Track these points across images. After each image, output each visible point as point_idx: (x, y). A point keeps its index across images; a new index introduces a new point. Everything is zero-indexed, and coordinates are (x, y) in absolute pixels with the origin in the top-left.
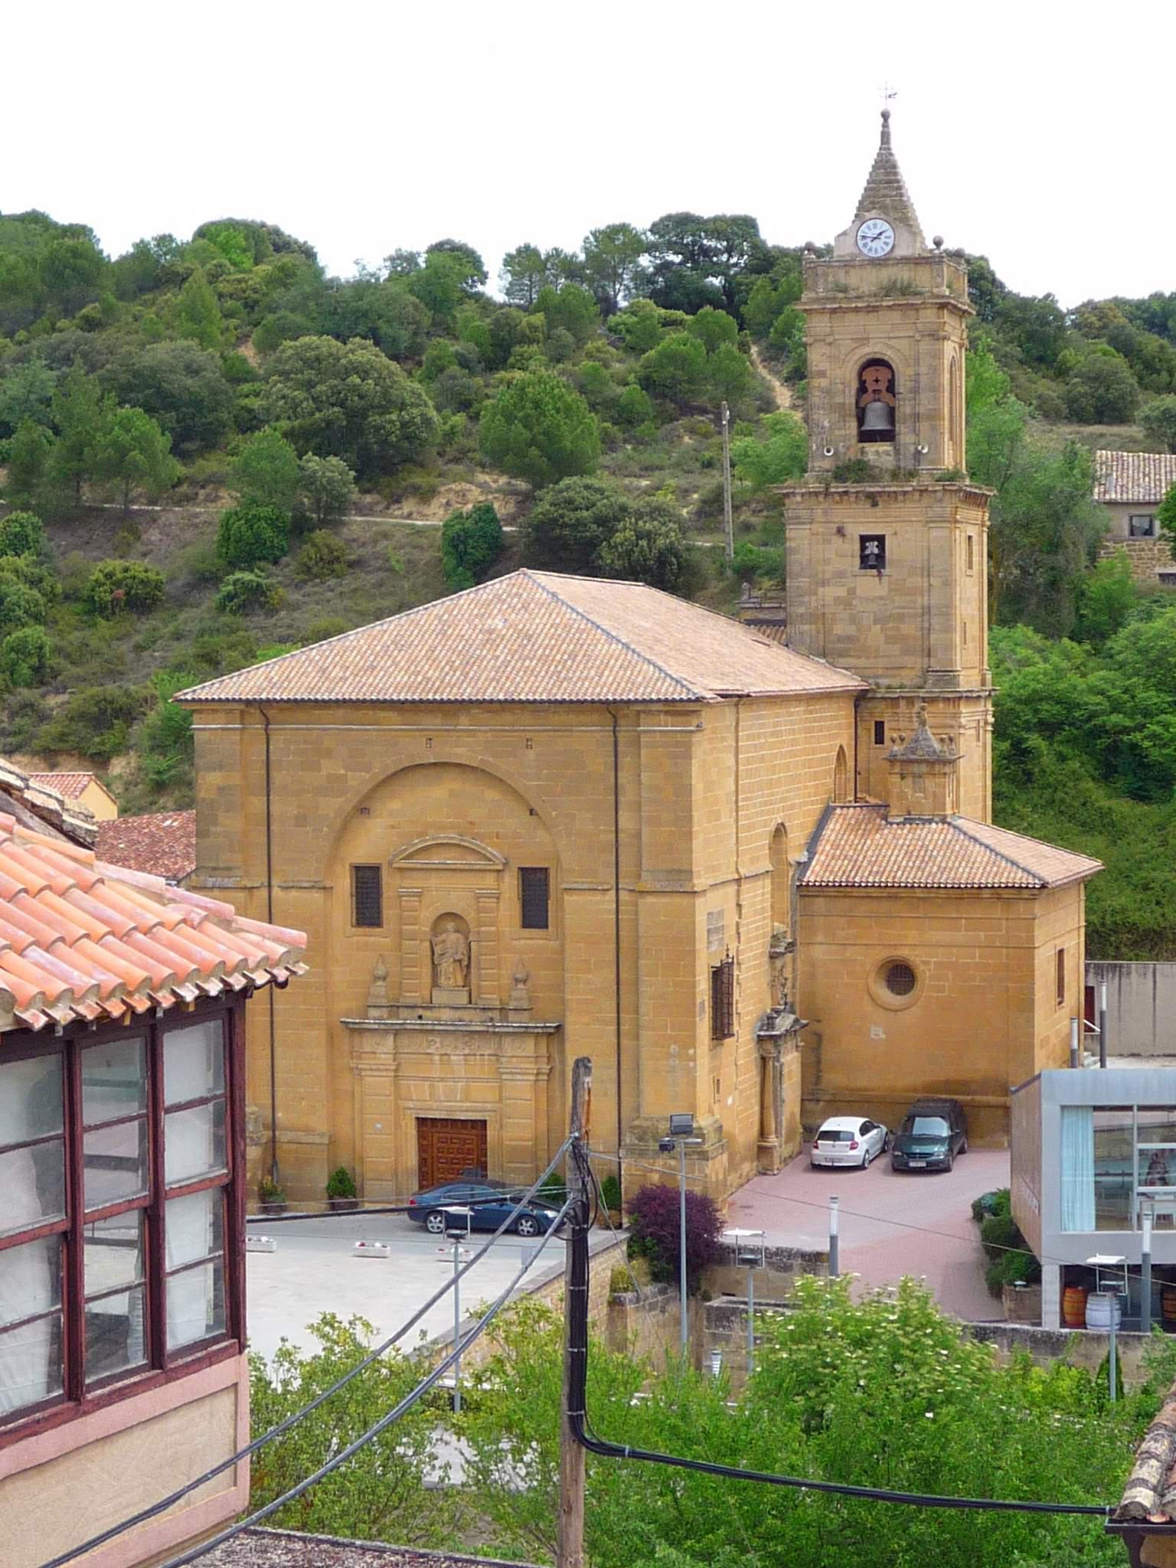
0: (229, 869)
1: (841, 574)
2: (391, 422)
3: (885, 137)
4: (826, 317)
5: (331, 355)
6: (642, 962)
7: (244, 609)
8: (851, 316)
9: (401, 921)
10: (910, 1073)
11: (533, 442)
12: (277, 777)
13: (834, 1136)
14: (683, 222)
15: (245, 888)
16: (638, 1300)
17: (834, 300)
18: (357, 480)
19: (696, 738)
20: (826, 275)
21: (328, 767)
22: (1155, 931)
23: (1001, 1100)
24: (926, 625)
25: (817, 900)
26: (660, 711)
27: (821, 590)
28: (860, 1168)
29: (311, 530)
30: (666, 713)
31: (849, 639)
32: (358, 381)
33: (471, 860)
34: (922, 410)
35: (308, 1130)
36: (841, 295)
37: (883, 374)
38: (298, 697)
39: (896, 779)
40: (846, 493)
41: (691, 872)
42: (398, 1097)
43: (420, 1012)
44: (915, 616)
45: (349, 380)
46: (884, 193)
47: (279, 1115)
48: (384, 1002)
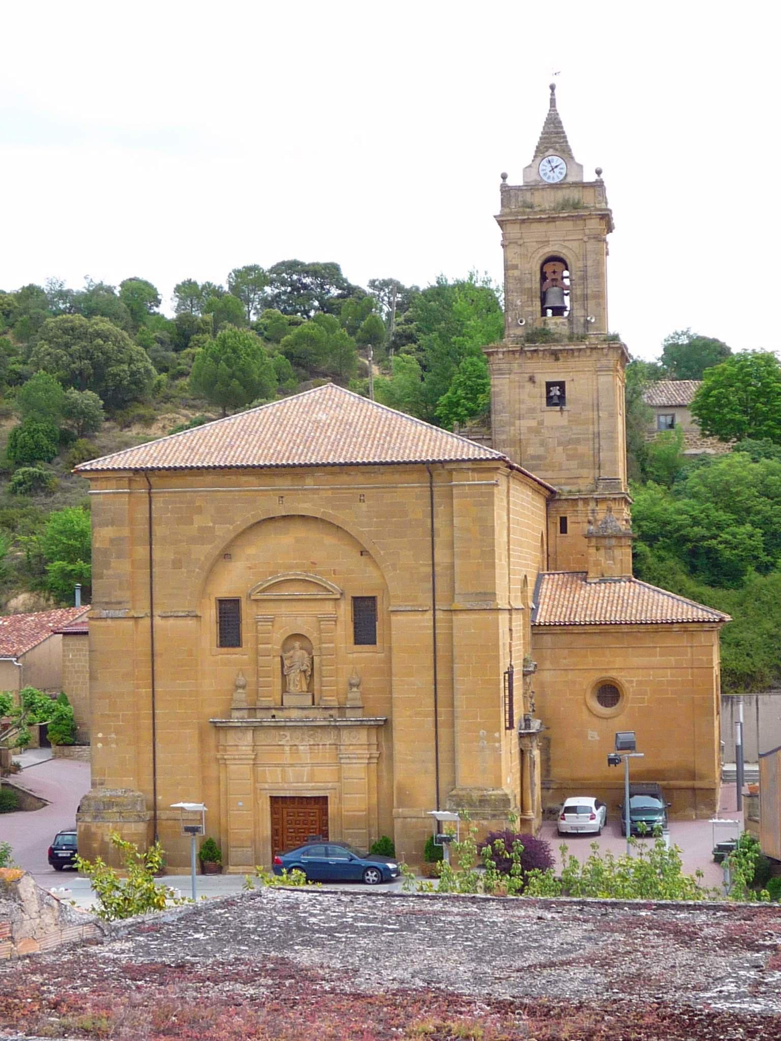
0: (120, 603)
1: (532, 410)
2: (124, 371)
3: (553, 102)
4: (517, 226)
5: (82, 326)
7: (29, 491)
8: (535, 226)
9: (257, 643)
11: (232, 376)
12: (158, 530)
13: (572, 810)
14: (292, 266)
15: (133, 618)
17: (524, 213)
18: (104, 407)
19: (496, 490)
20: (516, 196)
21: (199, 521)
22: (748, 674)
23: (689, 783)
24: (597, 446)
25: (545, 637)
26: (468, 469)
27: (517, 422)
28: (596, 834)
29: (74, 440)
30: (473, 470)
31: (539, 457)
32: (102, 342)
33: (313, 591)
34: (589, 292)
36: (528, 210)
38: (177, 465)
39: (592, 551)
40: (535, 351)
41: (495, 594)
42: (256, 781)
43: (274, 712)
44: (588, 440)
45: (95, 342)
47: (159, 798)
48: (244, 705)
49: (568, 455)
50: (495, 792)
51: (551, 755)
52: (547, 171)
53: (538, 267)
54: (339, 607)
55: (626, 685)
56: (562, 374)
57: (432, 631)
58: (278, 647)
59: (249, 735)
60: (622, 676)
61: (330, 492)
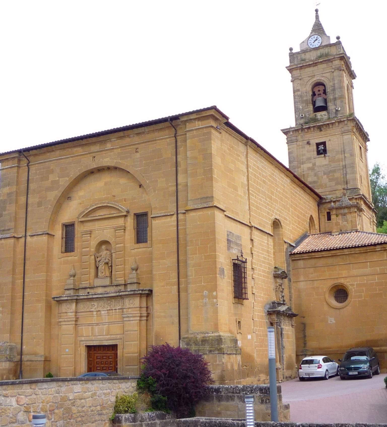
0: (9, 230)
1: (309, 159)
3: (317, 17)
6: (188, 248)
10: (349, 340)
12: (32, 186)
13: (311, 362)
16: (134, 420)
17: (300, 64)
20: (297, 57)
21: (52, 177)
24: (345, 172)
25: (299, 262)
27: (302, 166)
34: (337, 96)
35: (35, 354)
37: (322, 88)
43: (88, 290)
44: (340, 170)
46: (318, 29)
47: (24, 347)
49: (329, 179)
50: (212, 335)
51: (306, 334)
52: (312, 43)
53: (310, 89)
54: (127, 221)
55: (350, 287)
56: (324, 138)
57: (176, 228)
58: (93, 250)
59: (74, 305)
60: (347, 282)
61: (119, 149)
